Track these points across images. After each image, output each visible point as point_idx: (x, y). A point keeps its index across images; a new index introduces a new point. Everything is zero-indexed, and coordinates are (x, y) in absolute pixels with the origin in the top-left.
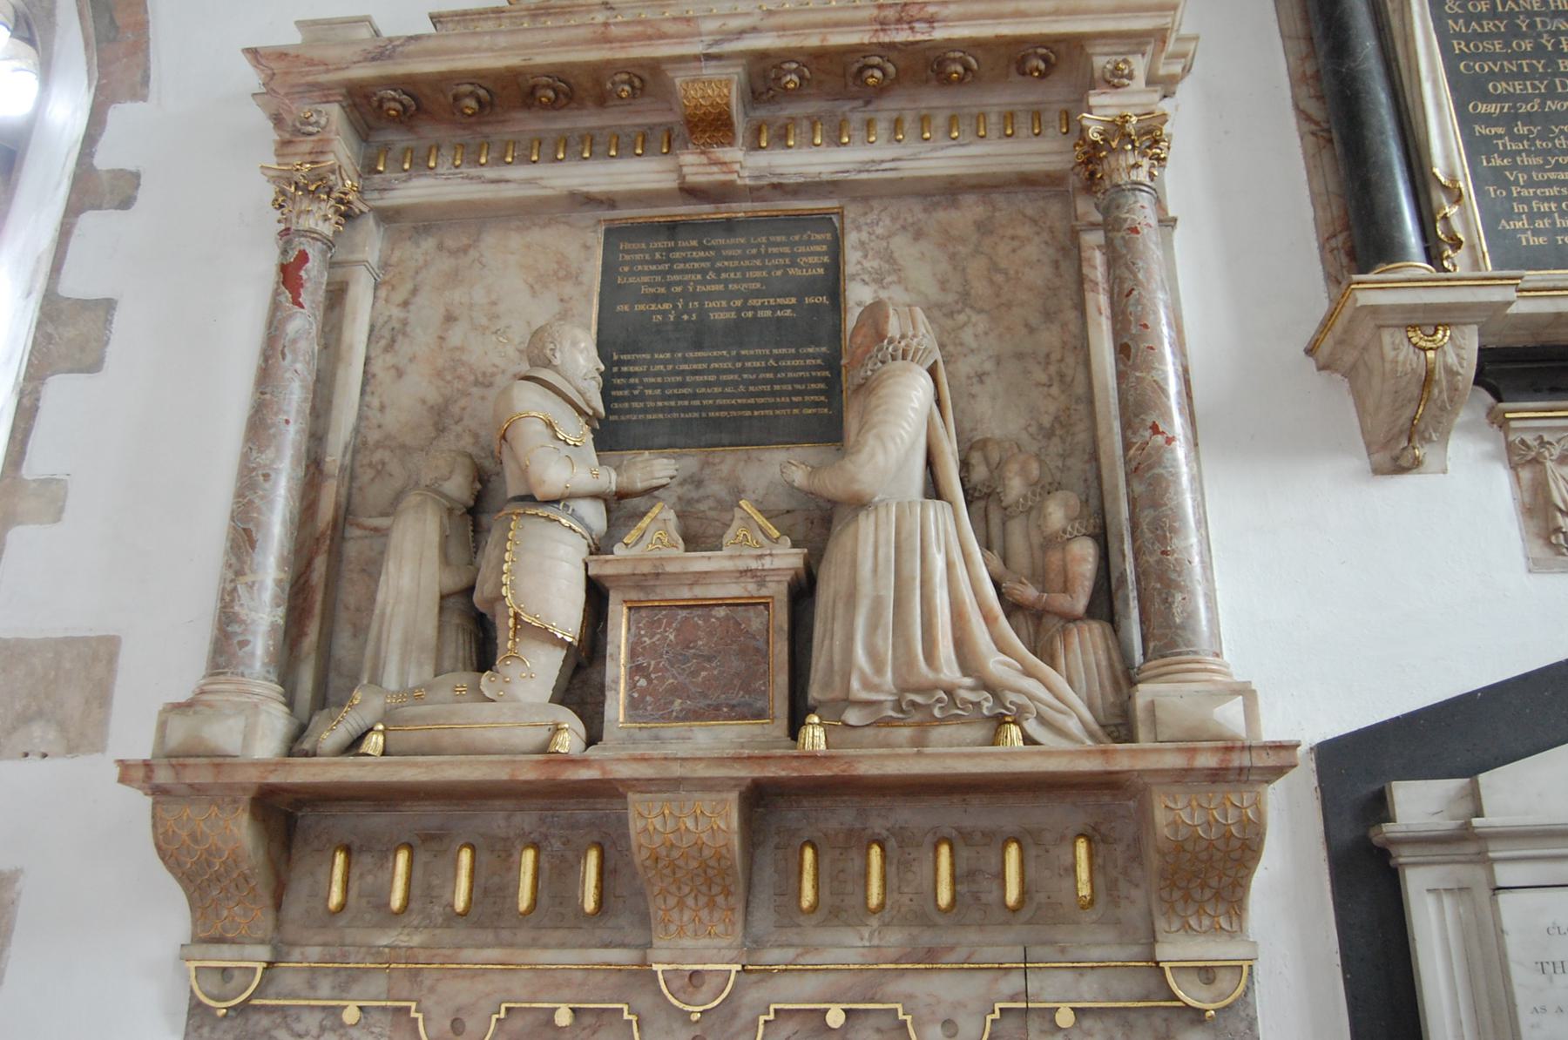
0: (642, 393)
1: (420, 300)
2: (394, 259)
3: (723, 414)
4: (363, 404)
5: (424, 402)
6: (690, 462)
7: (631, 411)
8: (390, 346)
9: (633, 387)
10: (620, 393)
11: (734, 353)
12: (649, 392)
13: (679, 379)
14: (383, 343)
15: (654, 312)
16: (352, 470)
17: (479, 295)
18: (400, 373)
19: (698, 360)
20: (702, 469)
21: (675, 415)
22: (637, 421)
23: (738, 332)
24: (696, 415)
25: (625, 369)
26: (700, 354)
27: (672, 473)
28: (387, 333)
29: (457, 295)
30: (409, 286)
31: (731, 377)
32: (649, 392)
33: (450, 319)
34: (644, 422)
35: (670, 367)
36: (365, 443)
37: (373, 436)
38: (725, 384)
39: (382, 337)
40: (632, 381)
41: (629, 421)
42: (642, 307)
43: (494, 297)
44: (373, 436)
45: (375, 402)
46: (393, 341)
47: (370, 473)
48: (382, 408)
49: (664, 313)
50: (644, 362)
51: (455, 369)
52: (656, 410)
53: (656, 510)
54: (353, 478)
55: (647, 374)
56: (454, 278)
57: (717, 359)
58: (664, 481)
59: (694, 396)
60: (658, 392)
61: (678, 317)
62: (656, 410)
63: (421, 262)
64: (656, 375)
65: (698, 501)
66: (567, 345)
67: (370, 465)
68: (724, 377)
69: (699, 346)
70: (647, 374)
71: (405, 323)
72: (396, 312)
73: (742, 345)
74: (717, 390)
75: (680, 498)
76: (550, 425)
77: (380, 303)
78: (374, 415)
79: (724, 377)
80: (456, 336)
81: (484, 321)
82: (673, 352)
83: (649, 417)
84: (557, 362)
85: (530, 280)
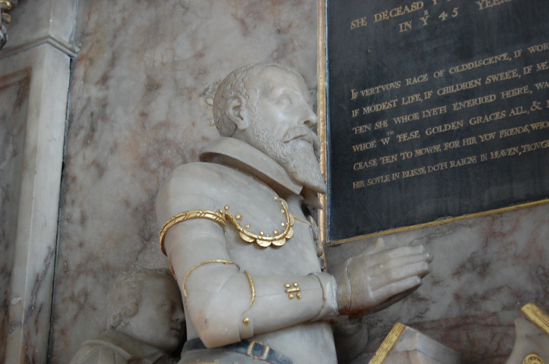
0: (394, 140)
1: (120, 71)
2: (92, 25)
3: (512, 151)
4: (62, 219)
5: (127, 203)
6: (463, 237)
7: (380, 170)
8: (89, 140)
9: (381, 134)
10: (363, 147)
11: (518, 53)
12: (403, 137)
13: (443, 109)
14: (82, 134)
15: (401, 19)
16: (53, 306)
17: (184, 49)
18: (100, 169)
19: (467, 76)
20: (486, 245)
21: (442, 165)
22: (391, 183)
23: (43, 43)
24: (472, 160)
25: (368, 110)
26: (469, 66)
27: (422, 266)
28: (85, 121)
29: (159, 55)
30: (107, 55)
31: (517, 92)
32: (403, 137)
33: (152, 86)
34: (398, 184)
35: (429, 94)
36: (66, 269)
37: (75, 258)
38: (512, 103)
39: (81, 127)
40: (379, 125)
41: (379, 186)
42: (384, 16)
43: (200, 46)
44: (75, 258)
45: (76, 215)
46: (93, 129)
47: (73, 308)
48: (83, 219)
49: (414, 17)
50: (393, 94)
51: (160, 152)
52: (415, 162)
53: (393, 336)
54: (53, 317)
55: (398, 111)
56: (154, 34)
57: (494, 69)
58: (409, 283)
59: (467, 131)
60: (415, 134)
61: (434, 18)
62: (415, 162)
63: (119, 22)
64: (414, 108)
65: (484, 297)
66: (255, 96)
67: (72, 298)
68: (507, 94)
69: (465, 54)
70: (398, 111)
71: (104, 104)
72: (95, 92)
73: (528, 39)
74: (498, 115)
75: (457, 297)
76: (227, 223)
77: (79, 83)
78: (73, 229)
79: (507, 94)
80: (159, 110)
81: (190, 82)
82: (430, 71)
83: (406, 174)
84: (243, 125)
85: (240, 13)
